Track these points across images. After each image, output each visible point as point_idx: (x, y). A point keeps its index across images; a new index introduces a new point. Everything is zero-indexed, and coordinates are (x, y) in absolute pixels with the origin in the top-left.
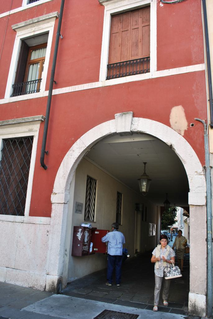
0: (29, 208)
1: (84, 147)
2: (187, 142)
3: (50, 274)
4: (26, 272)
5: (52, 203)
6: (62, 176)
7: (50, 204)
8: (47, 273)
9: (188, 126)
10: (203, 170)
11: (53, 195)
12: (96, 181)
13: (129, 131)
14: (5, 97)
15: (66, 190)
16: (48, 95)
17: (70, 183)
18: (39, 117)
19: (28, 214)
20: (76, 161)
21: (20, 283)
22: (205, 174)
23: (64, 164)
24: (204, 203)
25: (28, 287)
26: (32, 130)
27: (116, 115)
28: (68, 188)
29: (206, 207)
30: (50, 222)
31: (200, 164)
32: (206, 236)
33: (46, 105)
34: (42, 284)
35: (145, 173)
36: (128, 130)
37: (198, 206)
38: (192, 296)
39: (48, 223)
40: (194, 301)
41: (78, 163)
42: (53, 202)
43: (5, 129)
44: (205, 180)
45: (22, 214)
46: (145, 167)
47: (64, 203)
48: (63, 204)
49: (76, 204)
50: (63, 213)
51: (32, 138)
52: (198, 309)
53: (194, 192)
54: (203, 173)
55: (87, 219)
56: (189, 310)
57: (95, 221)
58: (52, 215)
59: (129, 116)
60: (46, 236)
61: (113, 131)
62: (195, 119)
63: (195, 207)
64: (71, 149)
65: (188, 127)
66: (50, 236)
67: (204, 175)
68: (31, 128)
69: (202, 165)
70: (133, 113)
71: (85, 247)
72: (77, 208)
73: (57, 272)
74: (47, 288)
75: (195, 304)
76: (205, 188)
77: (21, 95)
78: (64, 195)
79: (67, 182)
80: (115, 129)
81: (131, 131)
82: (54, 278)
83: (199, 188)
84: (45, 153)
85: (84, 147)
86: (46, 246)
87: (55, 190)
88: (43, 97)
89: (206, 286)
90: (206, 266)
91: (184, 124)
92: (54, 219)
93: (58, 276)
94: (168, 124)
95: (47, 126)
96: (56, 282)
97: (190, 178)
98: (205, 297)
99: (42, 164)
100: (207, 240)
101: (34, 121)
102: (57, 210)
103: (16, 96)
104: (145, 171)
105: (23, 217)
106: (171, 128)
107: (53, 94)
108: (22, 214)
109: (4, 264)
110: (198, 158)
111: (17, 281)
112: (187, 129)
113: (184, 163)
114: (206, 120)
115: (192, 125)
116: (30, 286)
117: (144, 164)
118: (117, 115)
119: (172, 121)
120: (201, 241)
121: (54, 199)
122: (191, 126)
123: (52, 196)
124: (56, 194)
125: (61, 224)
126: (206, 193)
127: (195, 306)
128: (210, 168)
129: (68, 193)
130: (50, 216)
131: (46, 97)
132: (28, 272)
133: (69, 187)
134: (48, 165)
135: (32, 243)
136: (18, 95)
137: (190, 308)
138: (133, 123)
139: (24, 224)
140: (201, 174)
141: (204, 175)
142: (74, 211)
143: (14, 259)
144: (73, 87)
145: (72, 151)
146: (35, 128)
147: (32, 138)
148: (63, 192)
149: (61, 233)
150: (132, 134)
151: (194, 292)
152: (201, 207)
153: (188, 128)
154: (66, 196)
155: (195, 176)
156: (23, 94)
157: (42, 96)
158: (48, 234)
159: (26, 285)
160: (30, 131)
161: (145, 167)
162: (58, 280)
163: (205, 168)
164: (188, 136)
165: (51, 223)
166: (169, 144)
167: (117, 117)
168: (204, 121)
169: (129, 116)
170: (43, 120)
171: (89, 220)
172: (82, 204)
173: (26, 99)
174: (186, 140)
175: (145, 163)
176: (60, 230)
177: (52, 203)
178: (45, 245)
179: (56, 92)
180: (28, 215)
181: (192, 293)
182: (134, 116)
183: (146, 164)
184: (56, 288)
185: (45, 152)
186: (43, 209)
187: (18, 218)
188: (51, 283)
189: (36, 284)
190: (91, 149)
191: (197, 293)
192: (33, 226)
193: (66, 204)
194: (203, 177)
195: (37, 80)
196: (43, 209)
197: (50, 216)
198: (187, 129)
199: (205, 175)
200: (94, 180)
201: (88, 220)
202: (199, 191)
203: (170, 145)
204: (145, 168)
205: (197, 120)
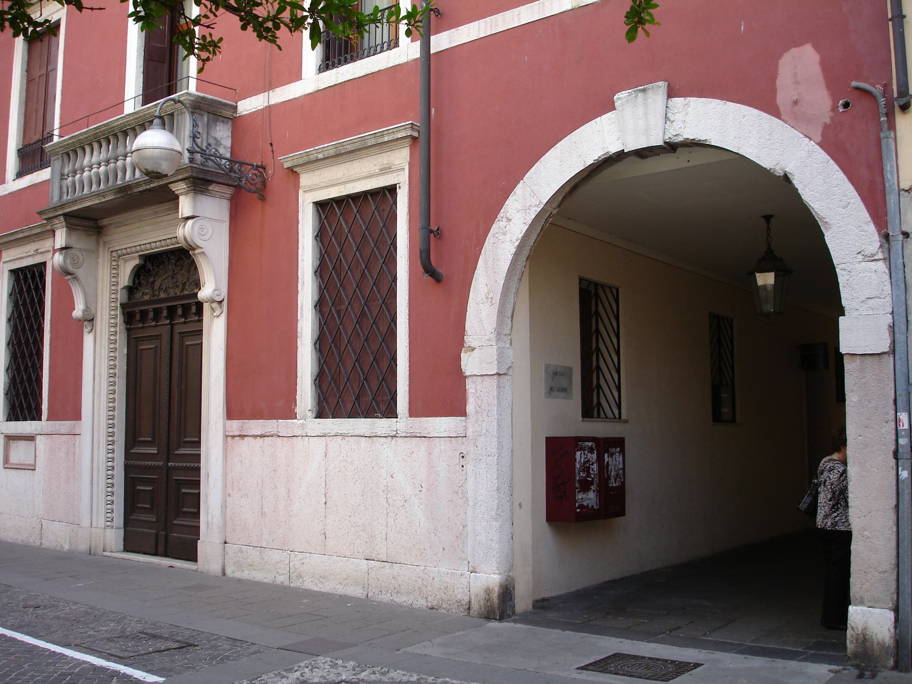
0: (407, 394)
1: (537, 206)
2: (832, 162)
3: (478, 570)
4: (418, 569)
5: (466, 377)
6: (484, 297)
7: (460, 379)
8: (471, 569)
9: (834, 108)
10: (881, 246)
11: (466, 352)
12: (617, 290)
13: (661, 143)
14: (304, 74)
15: (499, 334)
16: (418, 55)
17: (509, 314)
18: (402, 129)
19: (406, 411)
20: (519, 249)
21: (405, 598)
22: (887, 255)
23: (486, 263)
24: (885, 346)
25: (425, 608)
26: (394, 168)
27: (619, 99)
28: (507, 330)
29: (892, 358)
30: (466, 428)
31: (872, 228)
32: (894, 442)
33: (416, 82)
34: (459, 597)
35: (769, 252)
36: (656, 140)
37: (868, 357)
38: (856, 614)
39: (461, 432)
40: (860, 628)
41: (526, 252)
42: (467, 374)
43: (317, 173)
44: (887, 277)
45: (391, 413)
46: (768, 229)
47: (498, 374)
48: (495, 377)
49: (546, 372)
50: (499, 403)
51: (392, 190)
52: (873, 650)
53: (855, 314)
54: (880, 256)
55: (589, 410)
56: (848, 651)
57: (624, 416)
58: (470, 408)
59: (657, 93)
60: (458, 468)
61: (614, 149)
62: (854, 84)
63: (858, 360)
64: (501, 214)
65: (832, 114)
66: (469, 468)
67: (885, 259)
68: (385, 162)
69: (879, 231)
70: (668, 85)
71: (584, 496)
72: (555, 382)
73: (495, 564)
74: (475, 606)
75: (864, 637)
76: (889, 299)
77: (346, 62)
78: (494, 351)
79: (501, 312)
80: (620, 141)
81: (665, 143)
82: (490, 577)
83: (872, 301)
84: (432, 235)
85: (537, 206)
86: (461, 496)
87: (471, 339)
88: (407, 63)
89: (894, 587)
90: (895, 529)
91: (820, 102)
92: (476, 421)
93: (499, 574)
94: (772, 109)
95: (426, 146)
96: (496, 589)
97: (842, 272)
98: (891, 615)
99: (427, 268)
100: (896, 454)
101: (382, 146)
102: (479, 395)
103: (334, 66)
104: (769, 244)
105: (394, 420)
106: (781, 122)
107: (432, 52)
108: (391, 413)
109: (361, 550)
110: (865, 210)
111: (398, 592)
112: (828, 121)
113: (826, 228)
114: (885, 86)
115: (846, 105)
116: (430, 605)
117: (763, 220)
118: (621, 97)
119: (783, 98)
120: (880, 458)
121: (470, 363)
122: (841, 109)
123: (463, 356)
124: (473, 349)
125: (495, 434)
126: (891, 316)
127: (865, 640)
128: (901, 237)
129: (508, 345)
130: (463, 413)
131: (438, 32)
132: (422, 568)
133: (509, 327)
134: (444, 271)
135: (424, 490)
136: (340, 64)
137: (850, 646)
138: (669, 115)
139: (400, 440)
140: (876, 257)
141: (885, 259)
142: (543, 389)
143: (384, 537)
144: (488, 19)
145: (505, 220)
146: (397, 162)
147: (392, 190)
148: (491, 343)
149: (496, 458)
150: (671, 147)
151: (861, 603)
152: (876, 357)
153: (831, 118)
154: (501, 354)
155: (857, 265)
156: (353, 60)
157: (403, 60)
158: (462, 462)
159: (421, 603)
160: (385, 170)
161: (768, 229)
162: (501, 586)
163: (886, 237)
164: (834, 145)
165: (470, 433)
166: (780, 173)
167: (622, 104)
168: (877, 90)
169: (657, 93)
170: (416, 134)
171: (602, 415)
172: (570, 369)
173: (363, 74)
174: (829, 154)
175: (768, 218)
176: (495, 450)
177: (466, 377)
178: (460, 492)
179: (441, 42)
180: (407, 415)
181: (856, 605)
182: (671, 93)
183: (772, 220)
184: (496, 605)
185: (431, 231)
186: (444, 394)
187: (382, 425)
188: (482, 595)
189: (445, 597)
190: (559, 206)
191: (869, 604)
192: (424, 443)
193: (503, 377)
194: (881, 266)
195: (385, 9)
196: (444, 394)
197: (463, 413)
198: (828, 121)
199: (888, 260)
200: (610, 288)
201: (599, 416)
202: (871, 312)
203: (782, 174)
204: (768, 235)
205: (857, 88)
